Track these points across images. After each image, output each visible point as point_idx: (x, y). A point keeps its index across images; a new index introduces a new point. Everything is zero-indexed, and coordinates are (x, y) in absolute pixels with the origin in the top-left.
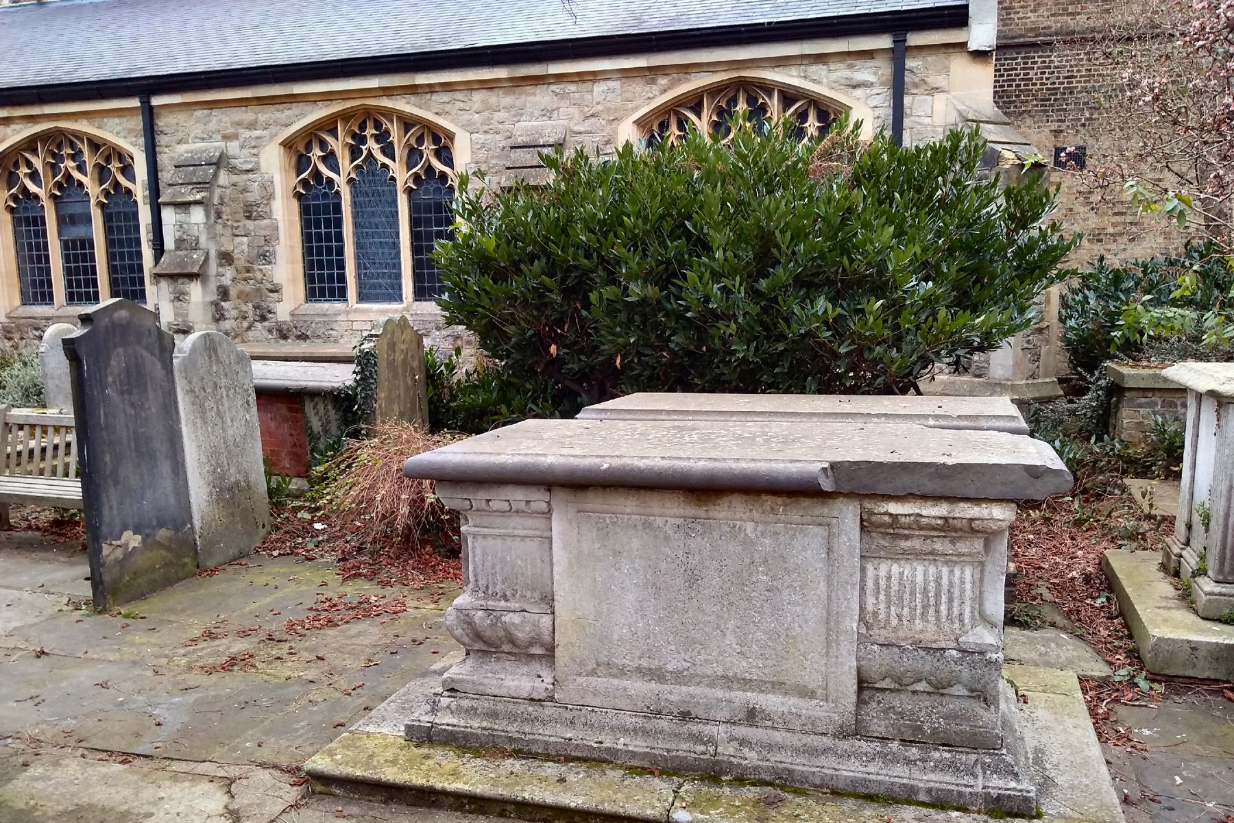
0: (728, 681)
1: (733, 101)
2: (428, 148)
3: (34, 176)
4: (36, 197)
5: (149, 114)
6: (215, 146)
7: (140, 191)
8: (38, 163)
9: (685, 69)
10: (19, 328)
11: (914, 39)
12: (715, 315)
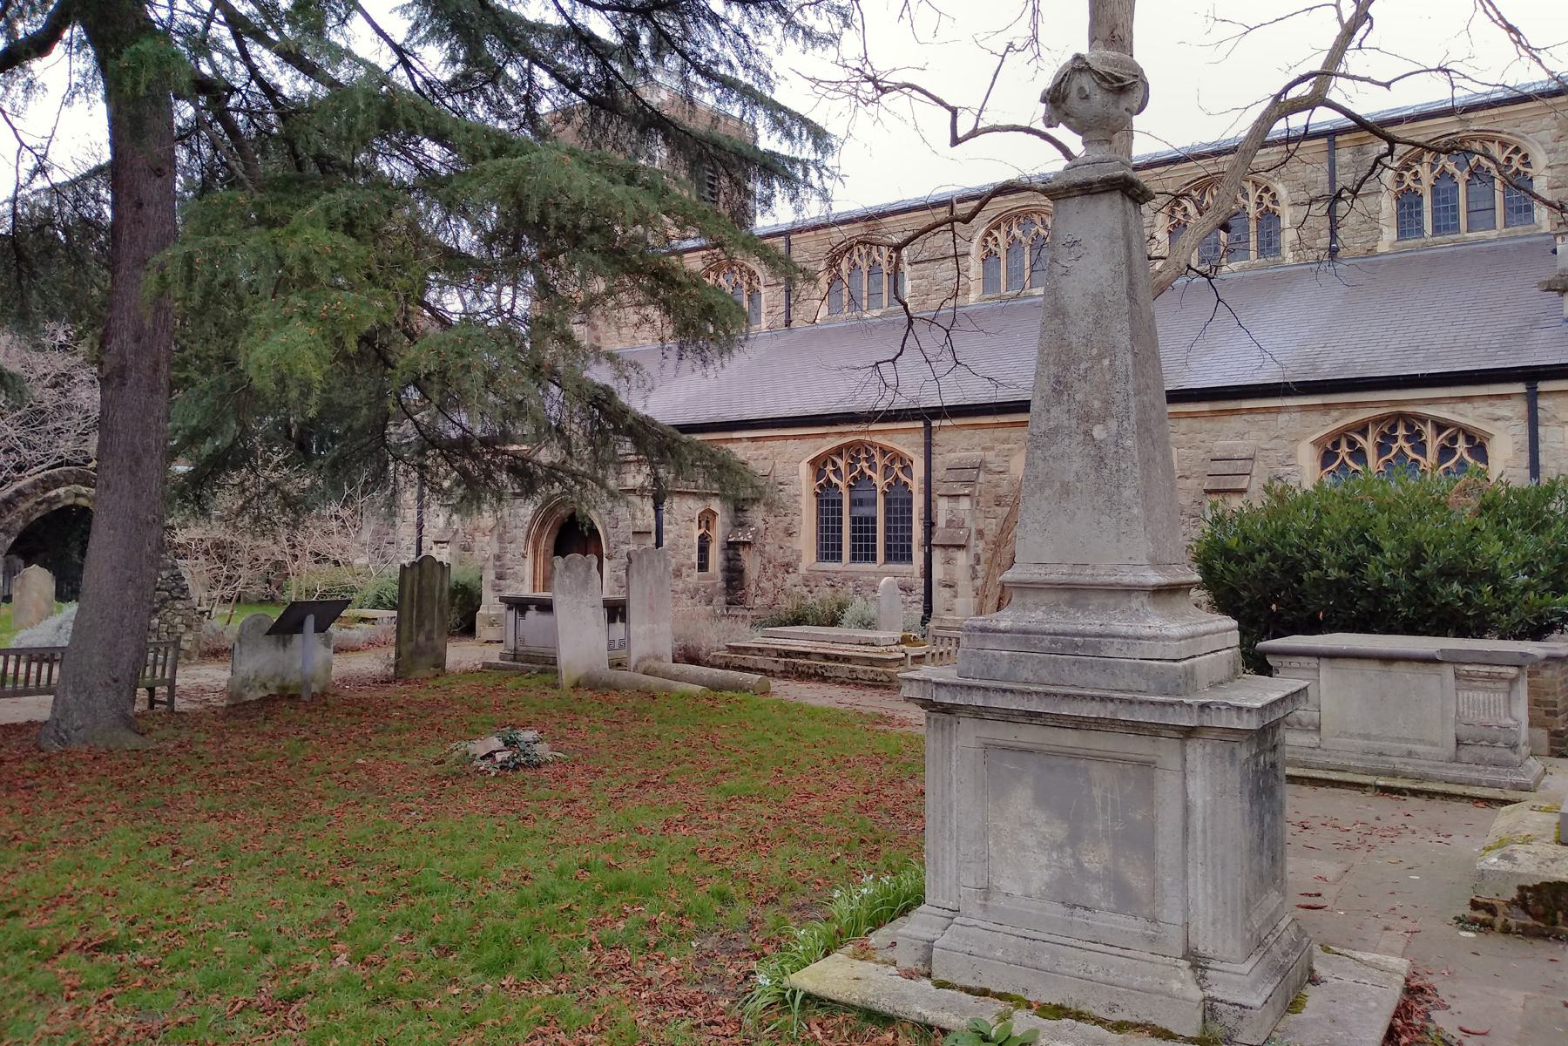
0: (1399, 739)
1: (1394, 428)
2: (1461, 446)
3: (837, 472)
4: (837, 486)
5: (929, 432)
6: (976, 455)
7: (916, 486)
8: (841, 464)
9: (1353, 405)
10: (815, 578)
11: (1543, 386)
12: (1387, 591)
